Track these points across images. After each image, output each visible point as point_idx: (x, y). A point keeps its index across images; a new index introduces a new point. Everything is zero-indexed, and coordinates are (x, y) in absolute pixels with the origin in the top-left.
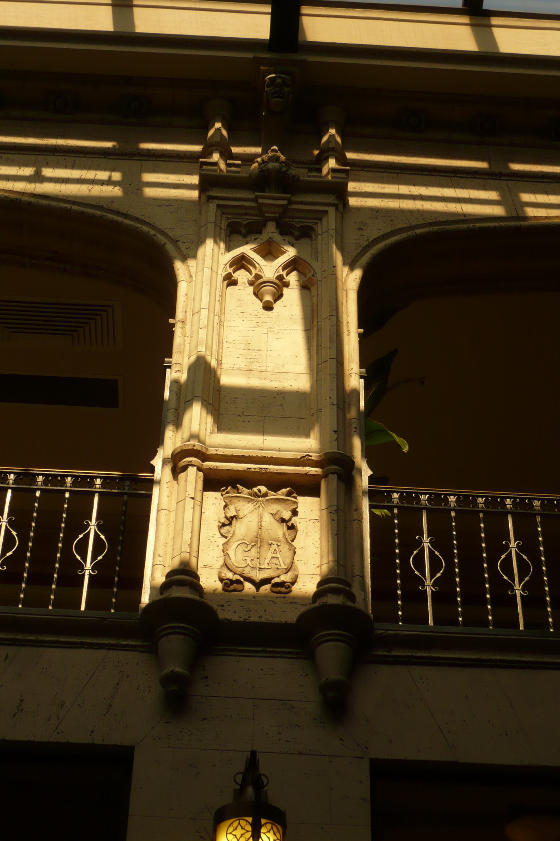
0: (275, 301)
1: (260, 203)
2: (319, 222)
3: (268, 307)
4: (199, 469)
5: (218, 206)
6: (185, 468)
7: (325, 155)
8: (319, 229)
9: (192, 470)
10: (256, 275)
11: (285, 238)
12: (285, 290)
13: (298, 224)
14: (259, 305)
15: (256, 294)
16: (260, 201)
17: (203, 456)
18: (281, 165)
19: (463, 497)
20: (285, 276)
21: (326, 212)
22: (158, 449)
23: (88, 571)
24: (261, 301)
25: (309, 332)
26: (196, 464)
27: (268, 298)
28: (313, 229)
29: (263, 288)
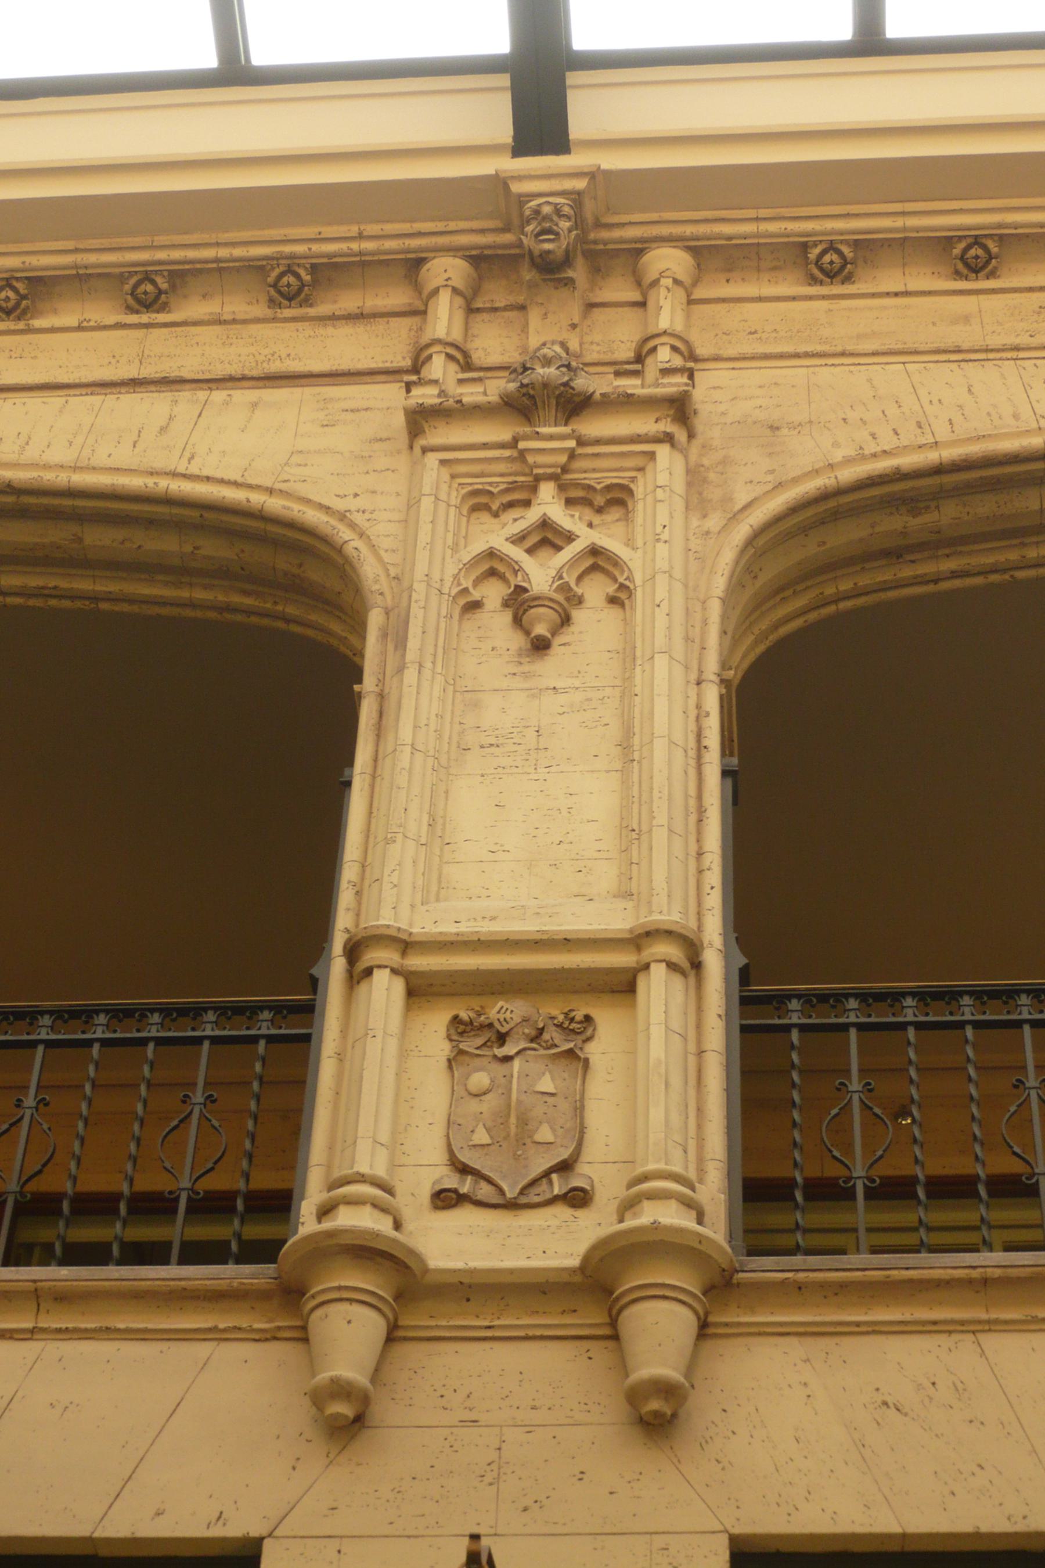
0: (553, 634)
1: (536, 475)
2: (639, 475)
3: (540, 646)
4: (394, 971)
5: (443, 462)
6: (368, 972)
7: (651, 344)
8: (639, 490)
9: (381, 977)
10: (517, 587)
11: (573, 513)
12: (576, 614)
13: (599, 483)
14: (517, 641)
15: (517, 621)
16: (522, 445)
17: (406, 945)
18: (561, 371)
19: (817, 999)
20: (573, 584)
21: (652, 456)
22: (324, 945)
23: (186, 1192)
24: (527, 633)
25: (559, 621)
26: (386, 964)
27: (541, 629)
28: (630, 492)
29: (533, 611)
